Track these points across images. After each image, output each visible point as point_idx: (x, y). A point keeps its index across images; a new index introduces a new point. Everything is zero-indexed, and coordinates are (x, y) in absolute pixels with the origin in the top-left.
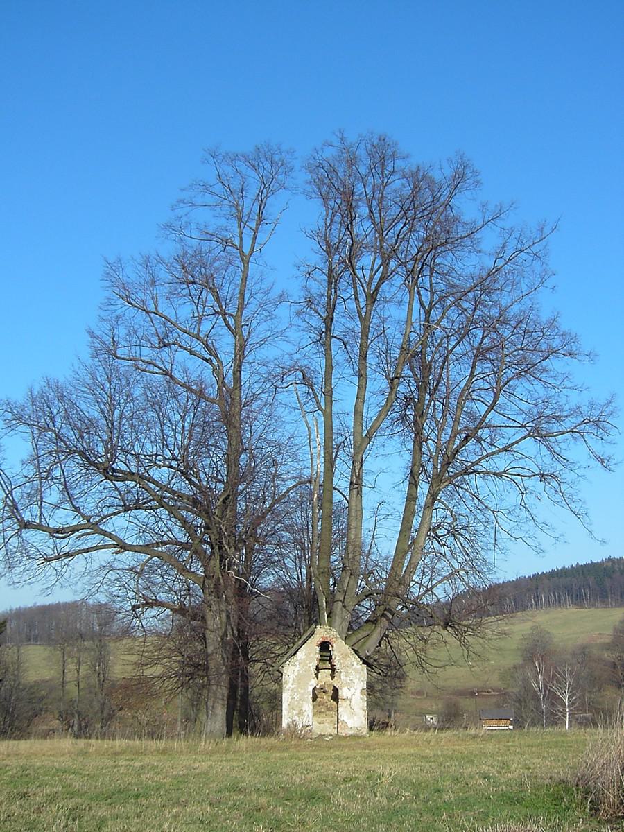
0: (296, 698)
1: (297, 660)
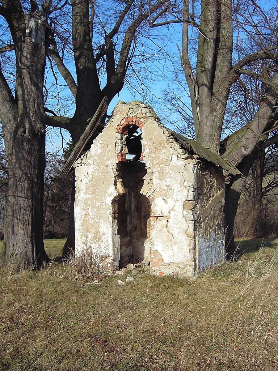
0: (91, 214)
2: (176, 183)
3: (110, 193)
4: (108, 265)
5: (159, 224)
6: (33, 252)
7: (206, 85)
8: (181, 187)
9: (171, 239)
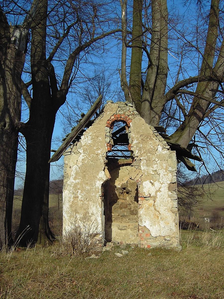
0: (80, 197)
1: (82, 146)
2: (162, 169)
3: (100, 178)
4: (97, 242)
5: (147, 203)
6: (6, 237)
7: (148, 101)
8: (166, 172)
9: (157, 216)
